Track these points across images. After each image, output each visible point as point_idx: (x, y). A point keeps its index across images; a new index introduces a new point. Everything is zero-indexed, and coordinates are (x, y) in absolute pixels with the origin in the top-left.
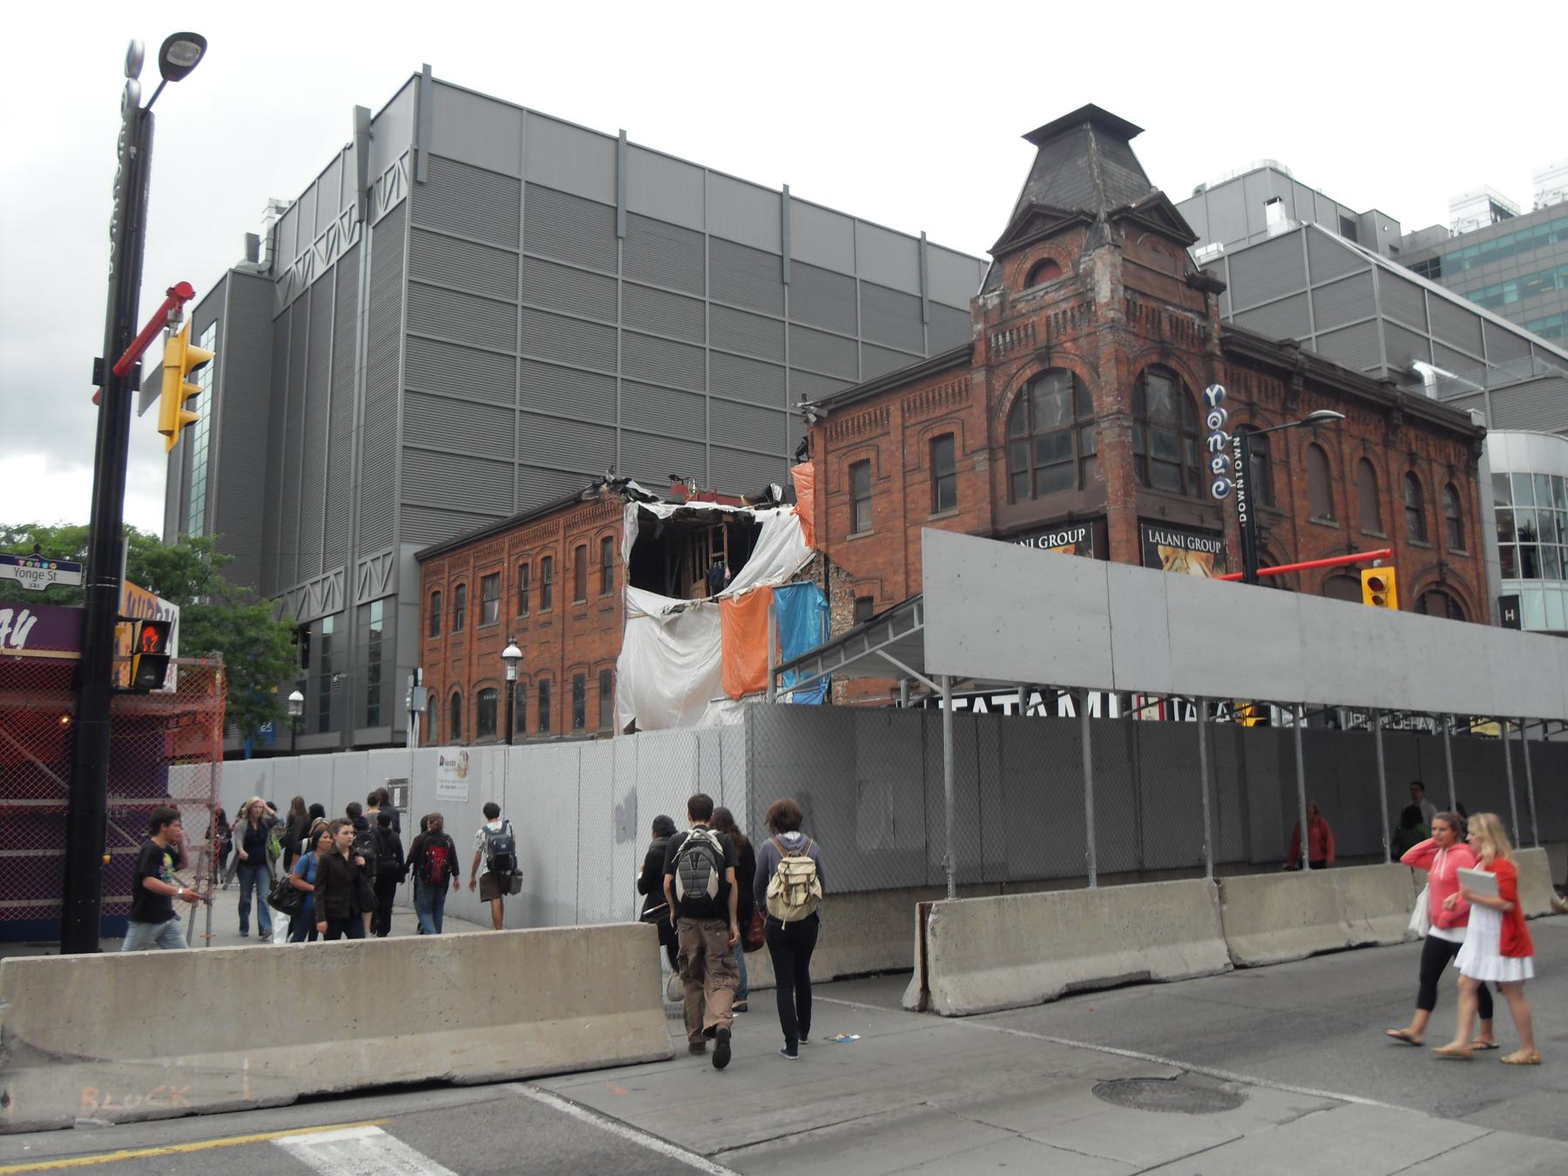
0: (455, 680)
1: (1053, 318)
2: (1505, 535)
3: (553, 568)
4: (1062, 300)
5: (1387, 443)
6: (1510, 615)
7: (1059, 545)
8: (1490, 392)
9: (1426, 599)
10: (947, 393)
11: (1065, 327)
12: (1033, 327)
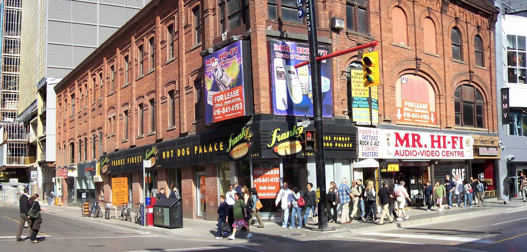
5: (443, 11)
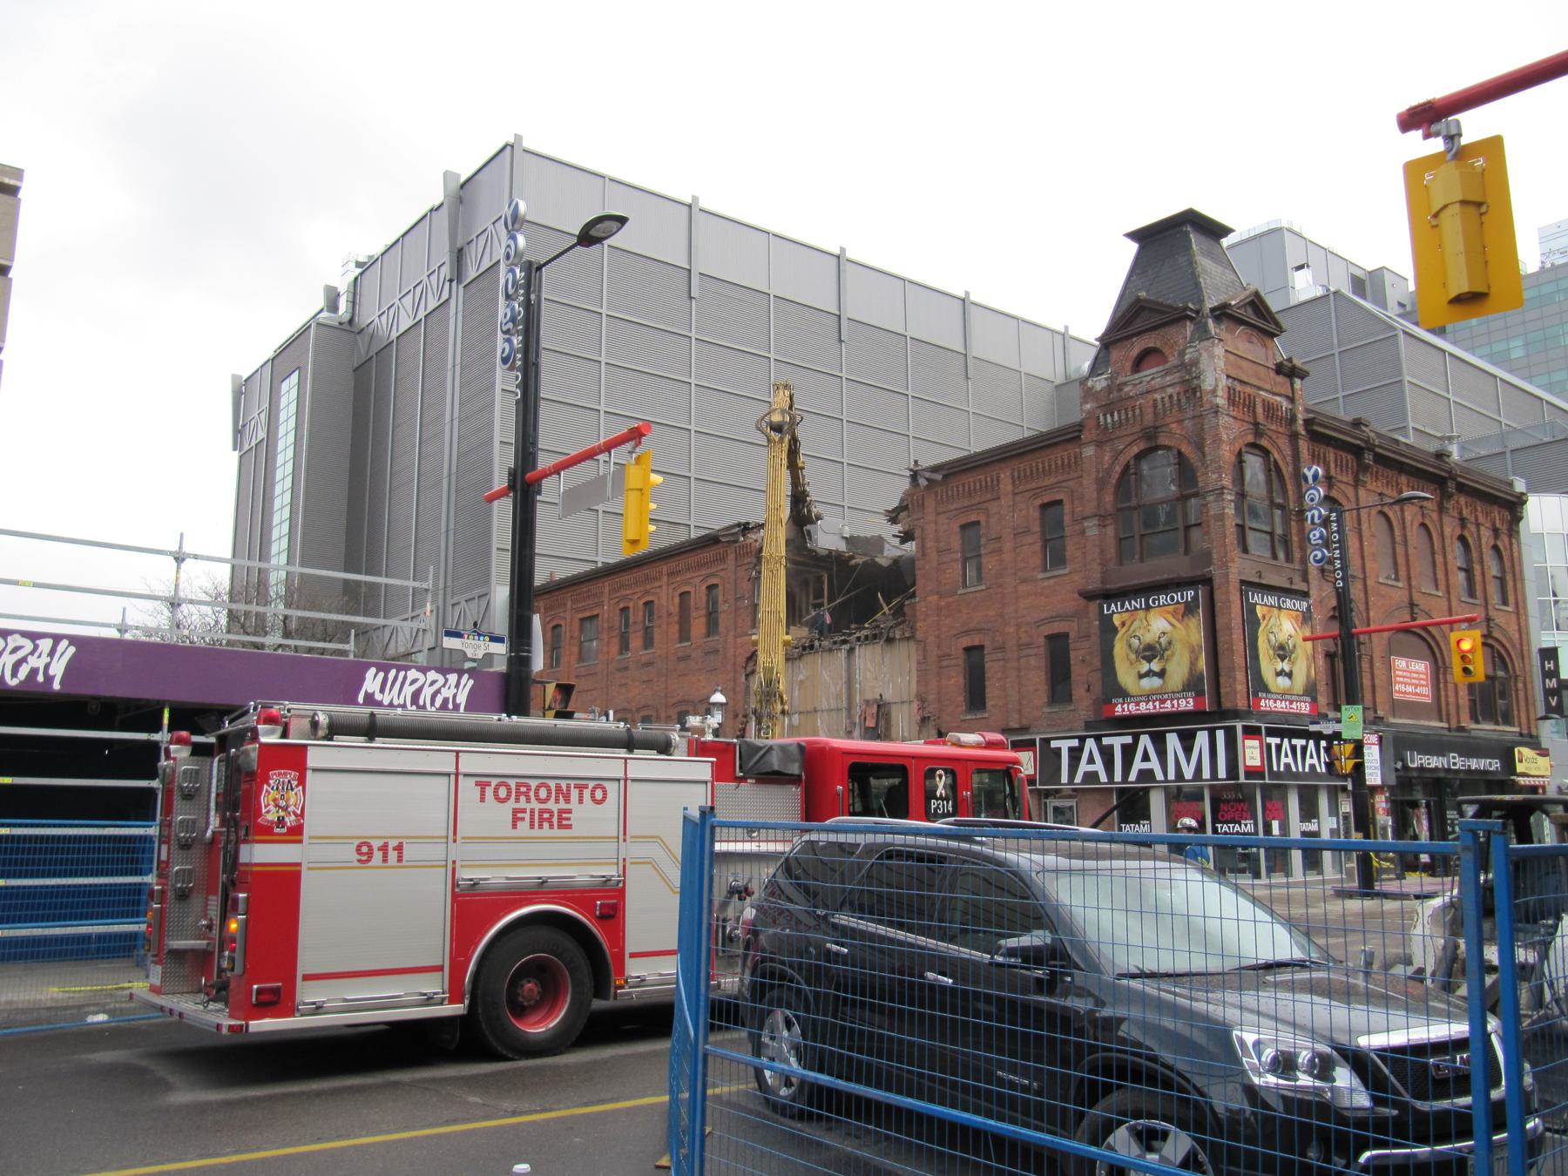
1: (1159, 401)
4: (1168, 386)
6: (1549, 665)
7: (1169, 605)
12: (1140, 408)
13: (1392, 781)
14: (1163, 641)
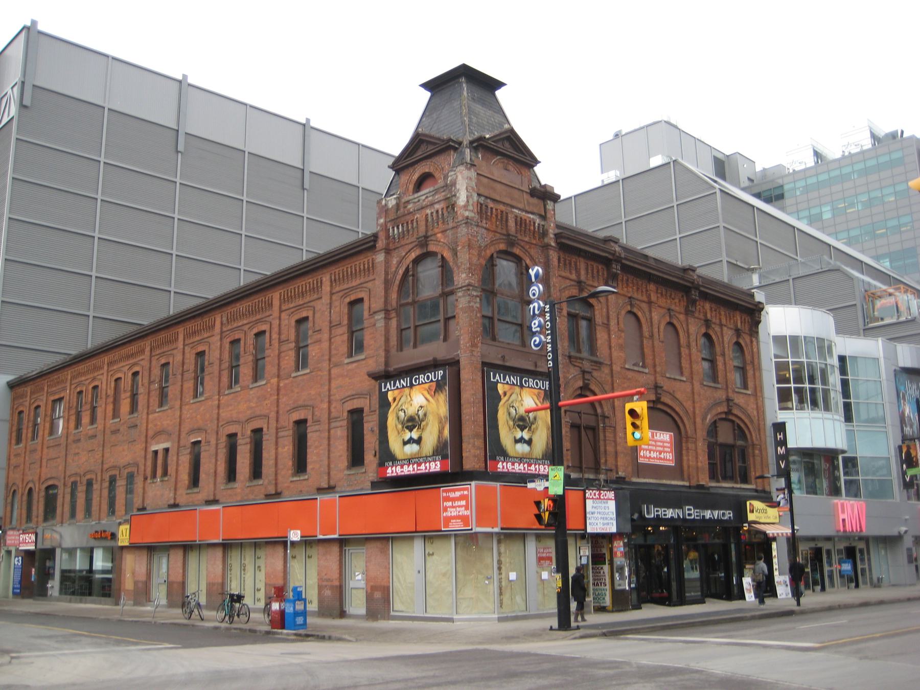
0: (30, 478)
2: (781, 379)
3: (99, 394)
5: (687, 312)
7: (426, 383)
8: (793, 279)
9: (717, 425)
10: (360, 268)
11: (438, 222)
12: (417, 222)
13: (628, 528)
14: (421, 413)
